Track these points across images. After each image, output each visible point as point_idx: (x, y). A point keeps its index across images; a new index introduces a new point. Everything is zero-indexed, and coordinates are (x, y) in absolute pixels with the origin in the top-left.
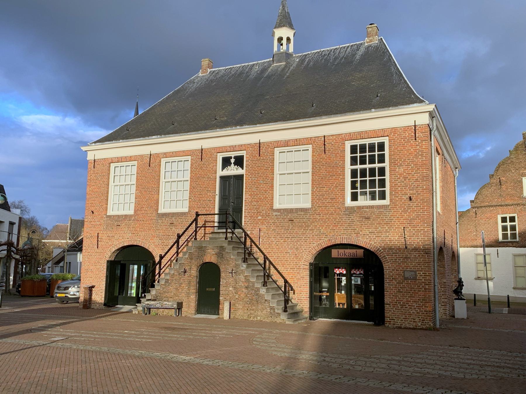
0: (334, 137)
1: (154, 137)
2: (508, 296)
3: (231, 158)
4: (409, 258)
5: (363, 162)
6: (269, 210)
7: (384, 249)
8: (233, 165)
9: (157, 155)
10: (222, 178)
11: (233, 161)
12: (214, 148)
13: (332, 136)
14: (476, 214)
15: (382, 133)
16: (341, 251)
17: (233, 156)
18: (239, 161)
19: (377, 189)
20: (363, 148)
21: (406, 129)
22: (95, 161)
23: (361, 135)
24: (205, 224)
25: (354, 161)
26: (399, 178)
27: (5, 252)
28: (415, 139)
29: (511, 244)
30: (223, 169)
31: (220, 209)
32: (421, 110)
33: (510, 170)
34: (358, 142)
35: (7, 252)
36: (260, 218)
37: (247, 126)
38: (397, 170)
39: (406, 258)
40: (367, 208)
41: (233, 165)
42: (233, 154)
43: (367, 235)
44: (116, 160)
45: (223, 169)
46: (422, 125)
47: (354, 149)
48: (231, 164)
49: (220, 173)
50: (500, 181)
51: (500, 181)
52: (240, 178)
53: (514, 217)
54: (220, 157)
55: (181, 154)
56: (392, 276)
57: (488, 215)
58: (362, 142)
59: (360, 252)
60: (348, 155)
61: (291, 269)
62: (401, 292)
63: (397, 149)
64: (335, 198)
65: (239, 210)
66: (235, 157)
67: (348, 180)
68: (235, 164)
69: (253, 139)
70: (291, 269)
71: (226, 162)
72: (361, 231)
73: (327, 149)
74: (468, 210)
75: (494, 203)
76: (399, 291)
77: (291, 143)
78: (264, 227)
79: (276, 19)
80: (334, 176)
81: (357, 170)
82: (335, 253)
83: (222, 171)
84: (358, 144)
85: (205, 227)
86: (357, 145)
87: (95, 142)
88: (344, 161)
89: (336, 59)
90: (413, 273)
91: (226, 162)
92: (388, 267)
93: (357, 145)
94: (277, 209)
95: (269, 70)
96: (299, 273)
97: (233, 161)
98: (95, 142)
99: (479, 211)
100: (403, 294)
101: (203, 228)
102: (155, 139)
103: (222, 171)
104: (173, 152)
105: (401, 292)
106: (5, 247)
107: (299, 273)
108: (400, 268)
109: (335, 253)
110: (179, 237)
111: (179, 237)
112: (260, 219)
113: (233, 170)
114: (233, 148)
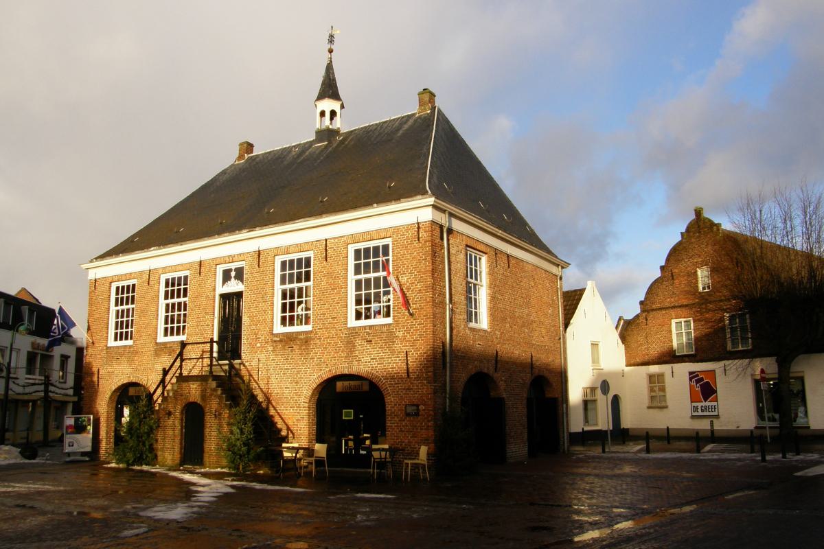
0: (336, 240)
1: (152, 249)
2: (668, 427)
3: (231, 270)
7: (386, 378)
8: (233, 279)
11: (233, 274)
13: (334, 238)
14: (647, 320)
15: (384, 233)
16: (346, 383)
18: (240, 274)
23: (364, 236)
24: (202, 355)
27: (42, 394)
28: (419, 240)
29: (687, 359)
32: (409, 206)
33: (683, 259)
34: (362, 246)
35: (45, 394)
36: (258, 345)
39: (408, 389)
41: (233, 279)
42: (233, 266)
43: (369, 362)
44: (116, 279)
45: (224, 283)
46: (426, 222)
47: (357, 252)
50: (672, 274)
51: (672, 274)
54: (220, 270)
55: (180, 268)
56: (394, 413)
57: (660, 321)
60: (351, 262)
61: (291, 407)
62: (404, 431)
63: (400, 253)
64: (336, 318)
65: (238, 338)
66: (236, 269)
68: (236, 277)
70: (291, 407)
72: (363, 358)
73: (329, 255)
74: (637, 316)
75: (667, 305)
76: (401, 431)
77: (291, 250)
78: (262, 357)
85: (203, 358)
86: (302, 258)
87: (96, 259)
88: (347, 270)
89: (380, 134)
90: (415, 408)
91: (227, 276)
92: (391, 402)
94: (277, 334)
95: (307, 153)
96: (299, 413)
97: (233, 274)
98: (102, 257)
99: (651, 315)
100: (405, 434)
101: (200, 360)
102: (154, 252)
103: (60, 306)
104: (125, 275)
105: (404, 431)
106: (42, 387)
107: (299, 413)
108: (402, 402)
109: (340, 385)
110: (165, 372)
111: (165, 372)
113: (234, 286)
114: (232, 259)
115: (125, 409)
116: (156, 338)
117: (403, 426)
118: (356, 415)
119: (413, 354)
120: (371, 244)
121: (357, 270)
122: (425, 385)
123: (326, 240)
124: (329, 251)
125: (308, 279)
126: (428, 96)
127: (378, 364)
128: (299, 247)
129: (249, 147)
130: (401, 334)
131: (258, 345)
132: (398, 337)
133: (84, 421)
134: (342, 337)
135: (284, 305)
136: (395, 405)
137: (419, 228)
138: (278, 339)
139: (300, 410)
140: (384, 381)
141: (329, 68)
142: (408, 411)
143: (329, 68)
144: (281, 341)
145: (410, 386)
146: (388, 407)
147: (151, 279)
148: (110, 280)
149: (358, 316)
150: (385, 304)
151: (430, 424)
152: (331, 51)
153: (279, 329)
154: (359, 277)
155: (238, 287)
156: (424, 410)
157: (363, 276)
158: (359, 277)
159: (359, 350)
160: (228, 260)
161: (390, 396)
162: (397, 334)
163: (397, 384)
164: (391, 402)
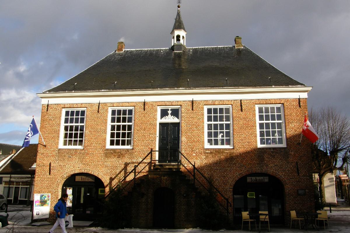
0: (248, 101)
4: (300, 181)
5: (119, 121)
6: (201, 149)
8: (170, 115)
9: (105, 104)
11: (170, 112)
17: (170, 109)
18: (175, 113)
19: (213, 138)
20: (215, 110)
21: (294, 100)
22: (48, 105)
25: (209, 119)
26: (292, 131)
30: (162, 117)
31: (159, 148)
36: (194, 155)
37: (168, 89)
38: (290, 125)
40: (226, 150)
41: (170, 115)
45: (162, 117)
52: (177, 125)
54: (159, 109)
58: (124, 108)
59: (266, 180)
60: (206, 115)
67: (206, 131)
68: (172, 114)
69: (96, 100)
71: (164, 113)
72: (270, 164)
73: (243, 109)
79: (172, 23)
81: (115, 125)
82: (249, 180)
83: (161, 119)
84: (224, 108)
91: (164, 113)
93: (127, 110)
96: (226, 194)
97: (170, 112)
103: (161, 119)
109: (249, 180)
112: (194, 156)
113: (170, 119)
115: (68, 190)
116: (105, 146)
117: (296, 201)
118: (257, 196)
119: (300, 163)
120: (122, 108)
121: (66, 121)
122: (308, 180)
123: (241, 100)
124: (243, 106)
125: (130, 120)
126: (237, 40)
127: (279, 168)
128: (222, 102)
129: (121, 45)
130: (293, 153)
131: (194, 155)
132: (291, 154)
133: (46, 197)
134: (255, 153)
135: (66, 134)
136: (291, 190)
137: (299, 101)
138: (210, 152)
139: (227, 193)
140: (283, 177)
141: (178, 14)
142: (299, 193)
143: (178, 14)
144: (211, 153)
145: (299, 180)
146: (287, 191)
147: (100, 109)
148: (63, 106)
149: (112, 143)
150: (221, 138)
151: (312, 199)
152: (179, 7)
153: (207, 146)
154: (67, 124)
155: (174, 120)
156: (308, 192)
157: (69, 124)
158: (67, 124)
159: (267, 161)
160: (168, 104)
161: (287, 185)
162: (290, 153)
163: (291, 178)
164: (288, 188)
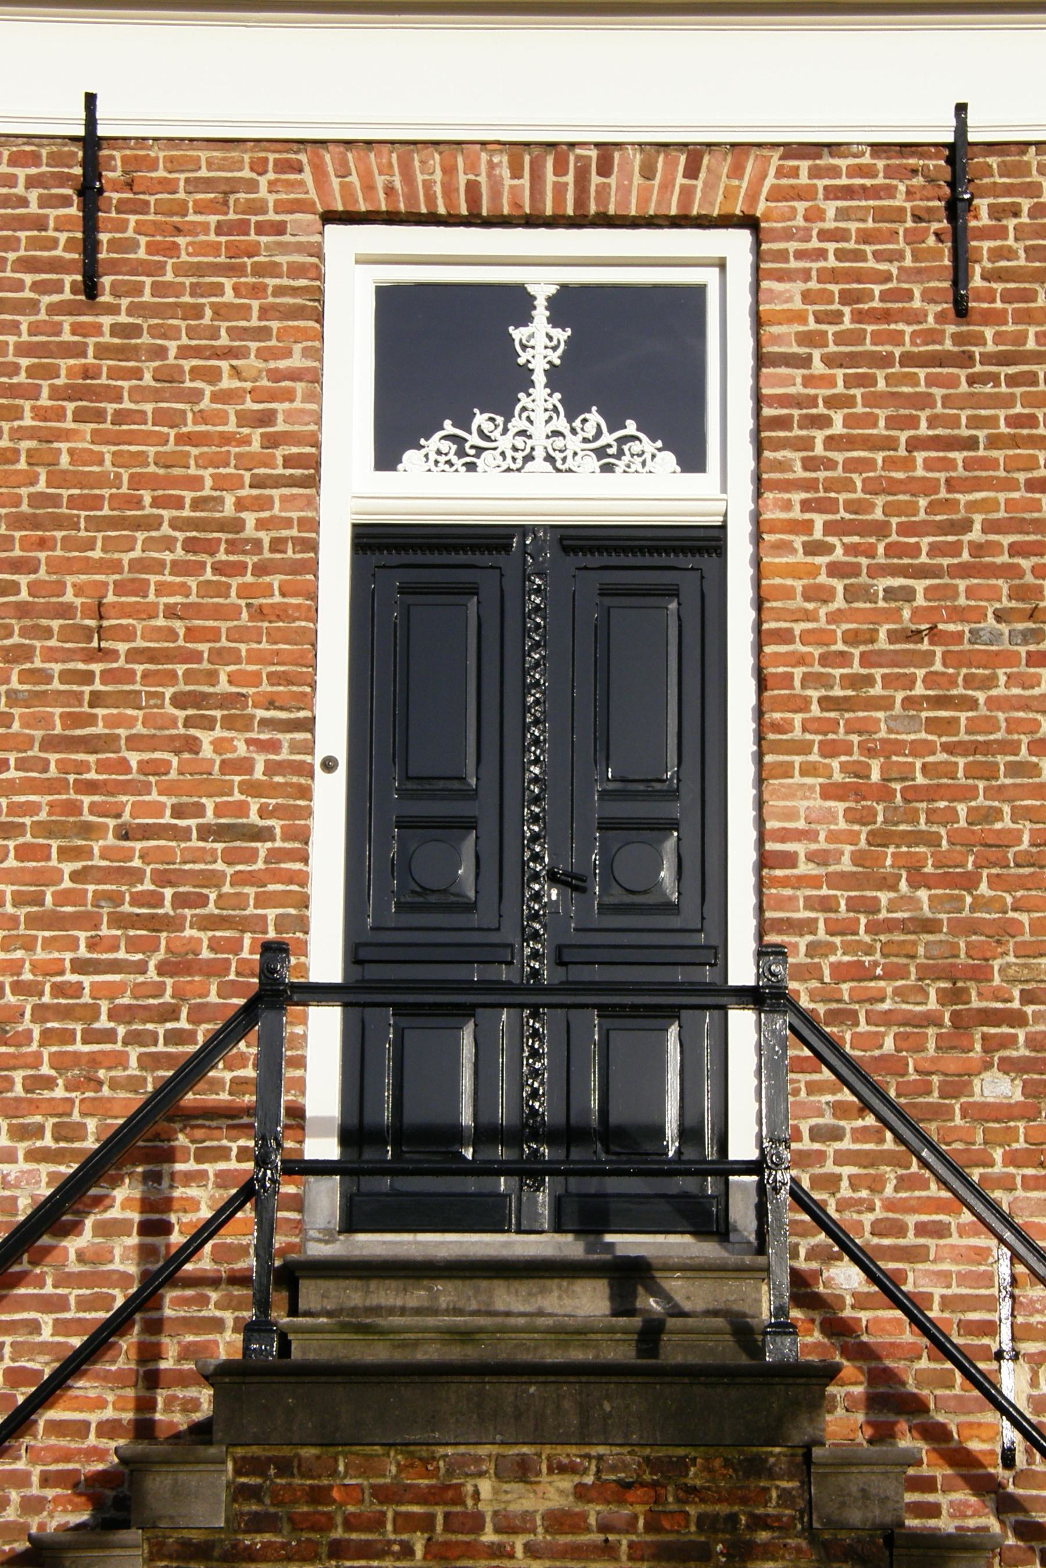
3: (515, 302)
8: (539, 399)
10: (370, 540)
11: (539, 342)
12: (291, 152)
17: (541, 285)
18: (636, 360)
31: (355, 953)
41: (539, 399)
42: (543, 261)
48: (523, 379)
49: (357, 488)
53: (679, 310)
54: (356, 270)
66: (568, 304)
71: (442, 359)
80: (90, 921)
91: (442, 359)
97: (539, 342)
113: (539, 473)
